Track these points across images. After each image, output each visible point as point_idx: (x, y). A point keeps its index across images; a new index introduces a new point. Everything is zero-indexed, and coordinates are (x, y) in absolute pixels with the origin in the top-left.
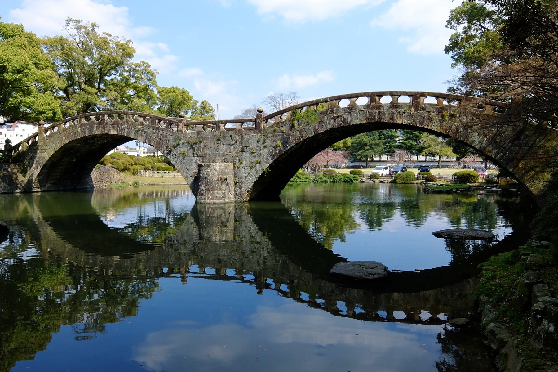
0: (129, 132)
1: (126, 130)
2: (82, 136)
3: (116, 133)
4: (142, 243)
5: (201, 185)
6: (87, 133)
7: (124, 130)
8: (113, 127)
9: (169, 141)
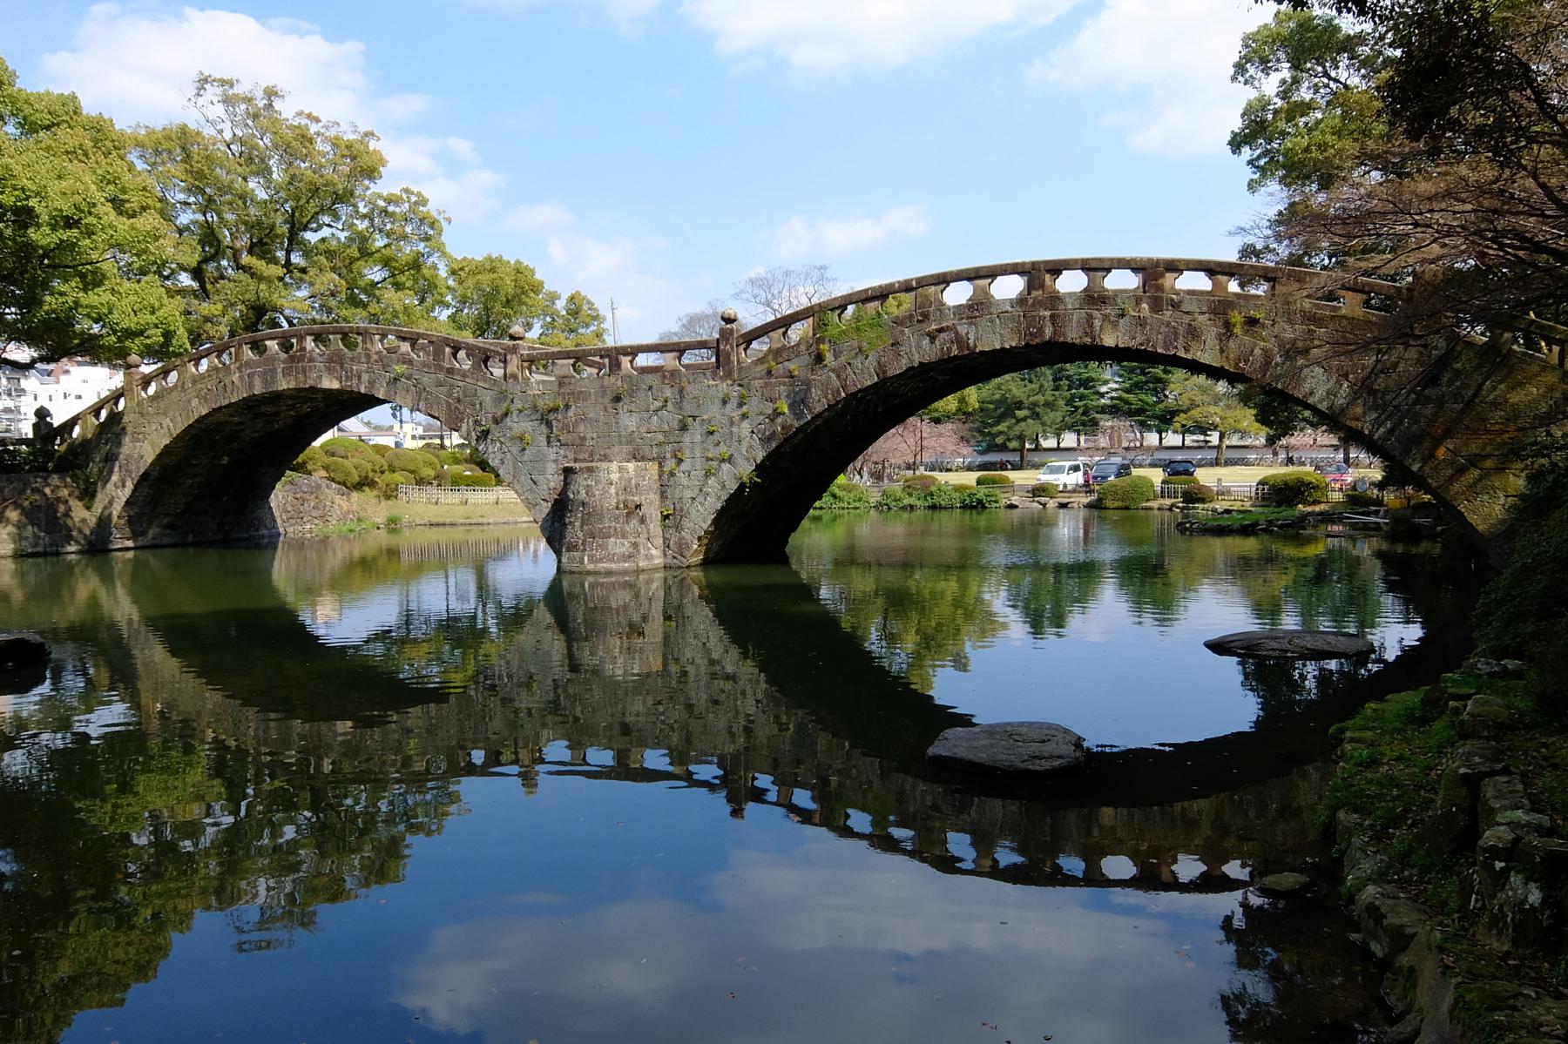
0: (372, 383)
2: (245, 395)
3: (336, 385)
5: (571, 522)
6: (257, 388)
8: (329, 370)
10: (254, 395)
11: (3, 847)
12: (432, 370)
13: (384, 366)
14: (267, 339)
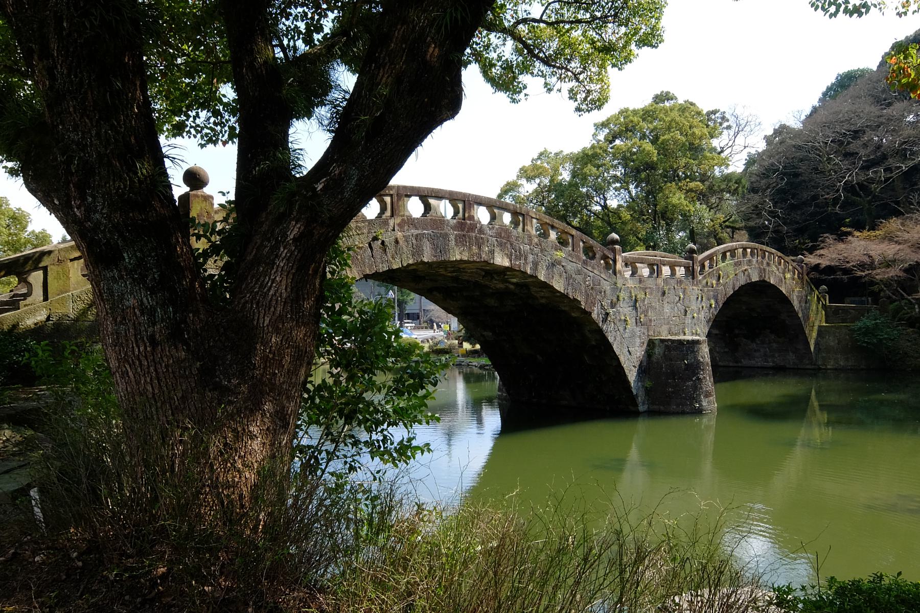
0: (535, 265)
1: (531, 258)
2: (411, 262)
3: (506, 263)
4: (769, 529)
5: (704, 377)
6: (426, 254)
7: (526, 259)
8: (501, 245)
9: (604, 292)
10: (423, 263)
11: (0, 428)
12: (574, 260)
13: (542, 251)
14: (432, 197)
